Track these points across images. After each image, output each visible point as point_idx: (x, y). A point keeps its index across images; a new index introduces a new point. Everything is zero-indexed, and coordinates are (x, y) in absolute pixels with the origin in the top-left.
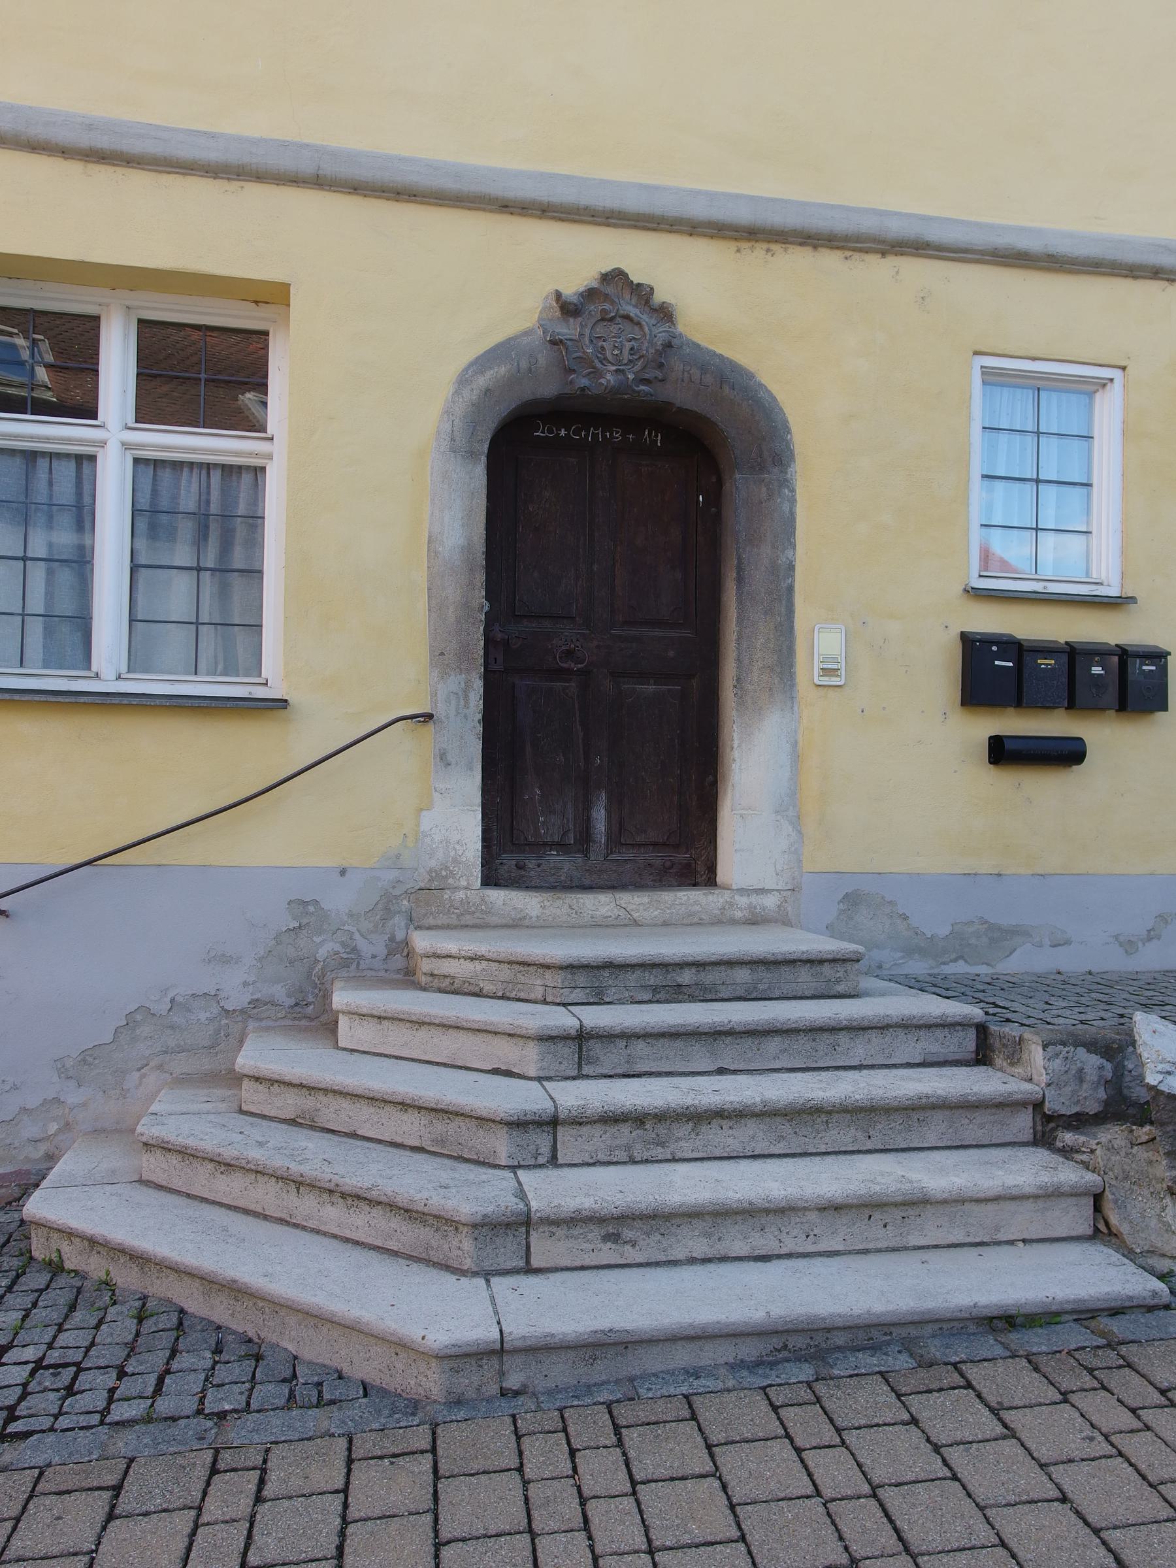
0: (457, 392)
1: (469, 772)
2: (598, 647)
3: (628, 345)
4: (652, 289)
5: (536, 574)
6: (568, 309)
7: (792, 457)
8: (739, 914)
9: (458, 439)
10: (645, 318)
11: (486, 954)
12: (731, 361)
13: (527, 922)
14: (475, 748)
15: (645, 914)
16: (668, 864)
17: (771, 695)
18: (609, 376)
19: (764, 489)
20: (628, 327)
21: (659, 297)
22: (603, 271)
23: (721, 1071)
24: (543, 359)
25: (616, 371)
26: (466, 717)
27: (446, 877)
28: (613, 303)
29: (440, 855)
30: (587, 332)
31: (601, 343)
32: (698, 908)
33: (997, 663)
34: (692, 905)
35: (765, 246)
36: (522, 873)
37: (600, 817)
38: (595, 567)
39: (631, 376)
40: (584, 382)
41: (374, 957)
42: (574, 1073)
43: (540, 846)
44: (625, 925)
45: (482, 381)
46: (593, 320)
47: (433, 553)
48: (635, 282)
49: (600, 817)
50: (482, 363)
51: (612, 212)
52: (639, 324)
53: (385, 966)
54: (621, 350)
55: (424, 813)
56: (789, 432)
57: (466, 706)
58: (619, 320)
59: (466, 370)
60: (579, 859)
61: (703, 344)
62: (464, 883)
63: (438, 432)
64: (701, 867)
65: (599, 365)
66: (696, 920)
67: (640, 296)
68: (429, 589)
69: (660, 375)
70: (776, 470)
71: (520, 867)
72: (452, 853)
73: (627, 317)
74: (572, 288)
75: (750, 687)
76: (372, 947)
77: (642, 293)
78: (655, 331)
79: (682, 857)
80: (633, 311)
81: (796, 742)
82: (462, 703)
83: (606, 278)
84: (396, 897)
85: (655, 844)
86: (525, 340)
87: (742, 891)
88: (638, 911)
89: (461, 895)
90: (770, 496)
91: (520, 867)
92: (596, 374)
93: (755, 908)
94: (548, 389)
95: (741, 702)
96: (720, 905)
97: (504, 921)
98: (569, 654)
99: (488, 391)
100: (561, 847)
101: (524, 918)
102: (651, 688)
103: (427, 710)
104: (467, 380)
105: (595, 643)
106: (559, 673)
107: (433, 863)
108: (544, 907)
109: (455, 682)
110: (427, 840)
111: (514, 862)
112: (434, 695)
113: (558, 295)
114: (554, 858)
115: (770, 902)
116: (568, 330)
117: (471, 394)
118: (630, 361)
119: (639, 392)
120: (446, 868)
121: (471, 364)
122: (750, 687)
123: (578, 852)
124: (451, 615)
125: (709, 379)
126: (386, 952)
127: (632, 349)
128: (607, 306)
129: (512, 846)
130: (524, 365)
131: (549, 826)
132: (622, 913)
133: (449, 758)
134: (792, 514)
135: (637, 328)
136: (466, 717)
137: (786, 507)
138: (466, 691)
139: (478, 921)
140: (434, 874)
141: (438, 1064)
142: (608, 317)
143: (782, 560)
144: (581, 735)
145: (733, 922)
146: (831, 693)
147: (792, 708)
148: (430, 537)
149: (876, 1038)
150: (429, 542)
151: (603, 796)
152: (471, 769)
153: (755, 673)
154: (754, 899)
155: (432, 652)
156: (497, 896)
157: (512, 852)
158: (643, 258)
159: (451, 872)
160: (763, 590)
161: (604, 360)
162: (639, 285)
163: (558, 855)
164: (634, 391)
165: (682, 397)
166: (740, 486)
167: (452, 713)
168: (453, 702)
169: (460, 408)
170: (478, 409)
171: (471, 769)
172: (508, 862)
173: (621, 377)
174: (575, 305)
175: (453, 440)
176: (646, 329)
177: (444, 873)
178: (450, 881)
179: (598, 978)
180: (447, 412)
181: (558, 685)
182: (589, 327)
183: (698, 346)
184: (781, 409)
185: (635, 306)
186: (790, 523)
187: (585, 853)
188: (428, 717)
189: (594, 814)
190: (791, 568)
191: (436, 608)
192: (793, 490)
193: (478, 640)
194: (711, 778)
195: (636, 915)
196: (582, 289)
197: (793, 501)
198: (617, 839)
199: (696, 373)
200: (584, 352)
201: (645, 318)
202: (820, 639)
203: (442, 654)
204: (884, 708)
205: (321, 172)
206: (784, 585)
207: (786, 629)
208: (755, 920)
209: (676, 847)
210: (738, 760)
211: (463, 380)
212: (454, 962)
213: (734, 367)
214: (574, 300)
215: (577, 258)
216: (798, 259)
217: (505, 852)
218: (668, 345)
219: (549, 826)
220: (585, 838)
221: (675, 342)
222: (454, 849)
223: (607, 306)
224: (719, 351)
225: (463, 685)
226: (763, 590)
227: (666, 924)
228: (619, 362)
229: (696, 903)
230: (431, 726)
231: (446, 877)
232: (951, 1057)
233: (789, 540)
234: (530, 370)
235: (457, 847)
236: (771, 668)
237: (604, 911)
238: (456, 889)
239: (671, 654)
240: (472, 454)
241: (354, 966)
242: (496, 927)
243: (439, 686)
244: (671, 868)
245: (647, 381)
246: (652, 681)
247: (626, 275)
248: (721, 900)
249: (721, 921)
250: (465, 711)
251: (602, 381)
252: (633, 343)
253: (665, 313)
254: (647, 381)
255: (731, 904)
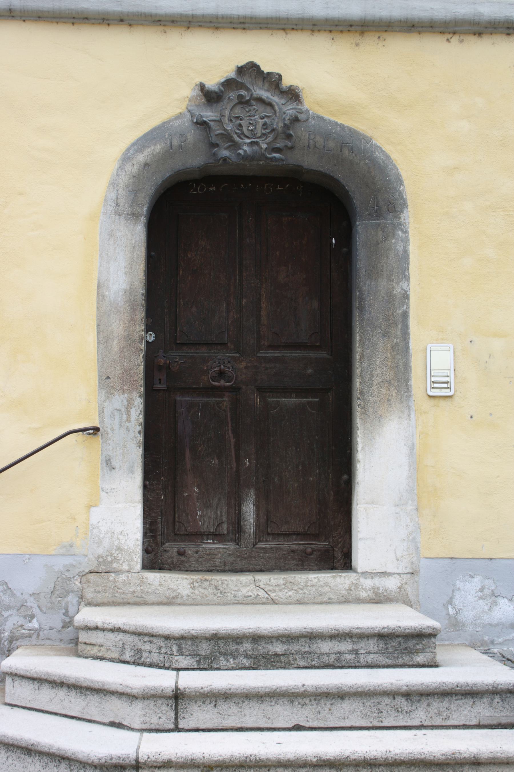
0: (121, 168)
1: (131, 475)
2: (246, 367)
3: (261, 122)
4: (280, 76)
5: (194, 309)
6: (210, 97)
7: (405, 205)
8: (363, 595)
9: (122, 204)
10: (276, 99)
11: (122, 627)
12: (350, 129)
13: (179, 601)
14: (136, 454)
15: (280, 594)
16: (309, 550)
17: (390, 405)
18: (245, 148)
19: (380, 233)
20: (260, 108)
21: (287, 82)
22: (239, 65)
23: (298, 728)
24: (192, 136)
25: (252, 143)
26: (128, 429)
27: (111, 562)
28: (248, 89)
29: (106, 543)
30: (227, 113)
31: (239, 122)
32: (327, 589)
33: (318, 400)
34: (322, 587)
35: (117, 633)
36: (183, 558)
37: (249, 510)
38: (244, 301)
39: (264, 146)
40: (225, 153)
41: (51, 629)
42: (172, 726)
43: (197, 536)
44: (264, 603)
45: (141, 158)
46: (232, 104)
47: (101, 296)
48: (265, 72)
49: (249, 510)
50: (141, 144)
51: (245, 17)
52: (270, 104)
53: (61, 637)
54: (255, 126)
55: (93, 509)
56: (402, 183)
57: (128, 420)
58: (253, 102)
59: (128, 150)
60: (232, 546)
61: (327, 116)
62: (126, 567)
63: (106, 200)
64: (338, 555)
65: (237, 139)
66: (325, 599)
67: (271, 83)
68: (98, 326)
69: (289, 144)
70: (390, 215)
71: (181, 553)
72: (116, 543)
73: (260, 100)
74: (213, 82)
75: (372, 399)
76: (49, 621)
77: (273, 81)
78: (285, 109)
79: (322, 544)
80: (265, 94)
81: (413, 445)
82: (125, 417)
83: (240, 70)
84: (69, 579)
85: (297, 534)
86: (176, 123)
87: (365, 574)
88: (275, 591)
89: (123, 577)
90: (386, 238)
91: (181, 553)
92: (235, 146)
93: (378, 589)
94: (196, 160)
95: (365, 412)
96: (347, 586)
97: (160, 600)
98: (221, 374)
99: (146, 165)
100: (217, 536)
101: (177, 597)
102: (292, 401)
103: (97, 424)
104: (129, 158)
105: (244, 364)
106: (219, 391)
107: (100, 551)
108: (193, 588)
109: (119, 400)
110: (95, 531)
111: (176, 549)
112: (101, 412)
113: (202, 87)
114: (210, 545)
115: (391, 584)
116: (209, 114)
117: (132, 169)
118: (264, 134)
119: (272, 159)
120: (111, 555)
121: (133, 145)
122: (372, 399)
123: (231, 540)
124: (115, 345)
125: (331, 144)
126: (61, 625)
127: (265, 124)
128: (243, 92)
129: (168, 538)
130: (176, 142)
131: (205, 517)
132: (261, 593)
133: (114, 463)
134: (406, 252)
135: (269, 109)
136: (128, 429)
137: (400, 246)
138: (128, 408)
139: (138, 600)
140: (101, 560)
141: (72, 717)
142: (244, 100)
143: (397, 291)
144: (233, 441)
145: (359, 601)
146: (443, 403)
147: (409, 415)
148: (99, 284)
149: (436, 704)
150: (99, 288)
151: (252, 492)
152: (132, 472)
153: (375, 387)
154: (377, 582)
155: (100, 376)
156: (154, 578)
157: (174, 541)
158: (271, 54)
159: (115, 558)
160: (380, 317)
161: (242, 135)
162: (269, 73)
163: (213, 543)
164: (267, 158)
165: (309, 161)
166: (363, 231)
167: (117, 426)
168: (117, 418)
169: (124, 180)
170: (138, 179)
171: (132, 472)
172: (172, 549)
173: (255, 148)
174: (216, 93)
175: (117, 205)
176: (276, 108)
177: (109, 559)
178: (115, 565)
179: (215, 649)
180: (113, 184)
181: (213, 400)
182: (229, 109)
183: (322, 119)
184: (395, 166)
185: (268, 90)
186: (405, 257)
187: (237, 541)
188: (96, 430)
189: (244, 508)
190: (406, 297)
191: (103, 339)
192: (406, 232)
193: (139, 365)
194: (345, 477)
195: (273, 595)
196: (223, 80)
197: (406, 241)
198: (264, 530)
199: (320, 140)
200: (225, 130)
201: (276, 99)
202: (433, 356)
203: (108, 378)
204: (491, 414)
205: (12, 7)
206: (399, 311)
207: (402, 349)
208: (379, 599)
209: (316, 537)
210: (362, 461)
211: (126, 158)
212: (100, 634)
213: (353, 133)
214: (215, 88)
215: (217, 58)
216: (401, 46)
217: (169, 541)
218: (296, 120)
219: (206, 516)
220: (237, 528)
221: (302, 117)
222: (118, 539)
223: (243, 92)
224: (339, 121)
225: (125, 403)
226: (380, 317)
227: (299, 602)
228: (254, 136)
229: (327, 584)
230: (99, 438)
231: (111, 562)
232: (504, 721)
233: (403, 273)
234: (180, 146)
235: (121, 537)
236: (389, 382)
237: (244, 591)
238: (118, 572)
239: (310, 371)
240: (134, 216)
241: (35, 636)
242: (153, 604)
243: (106, 404)
244: (311, 554)
245: (278, 150)
246: (294, 395)
247: (258, 67)
248: (348, 582)
249: (348, 599)
250: (128, 424)
251: (241, 152)
252: (266, 119)
253: (293, 95)
254: (278, 150)
255: (357, 586)
